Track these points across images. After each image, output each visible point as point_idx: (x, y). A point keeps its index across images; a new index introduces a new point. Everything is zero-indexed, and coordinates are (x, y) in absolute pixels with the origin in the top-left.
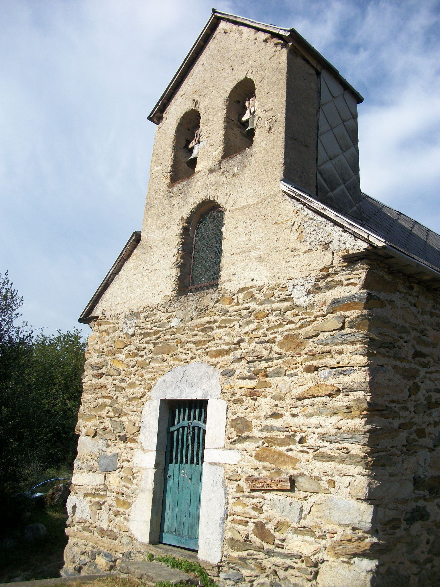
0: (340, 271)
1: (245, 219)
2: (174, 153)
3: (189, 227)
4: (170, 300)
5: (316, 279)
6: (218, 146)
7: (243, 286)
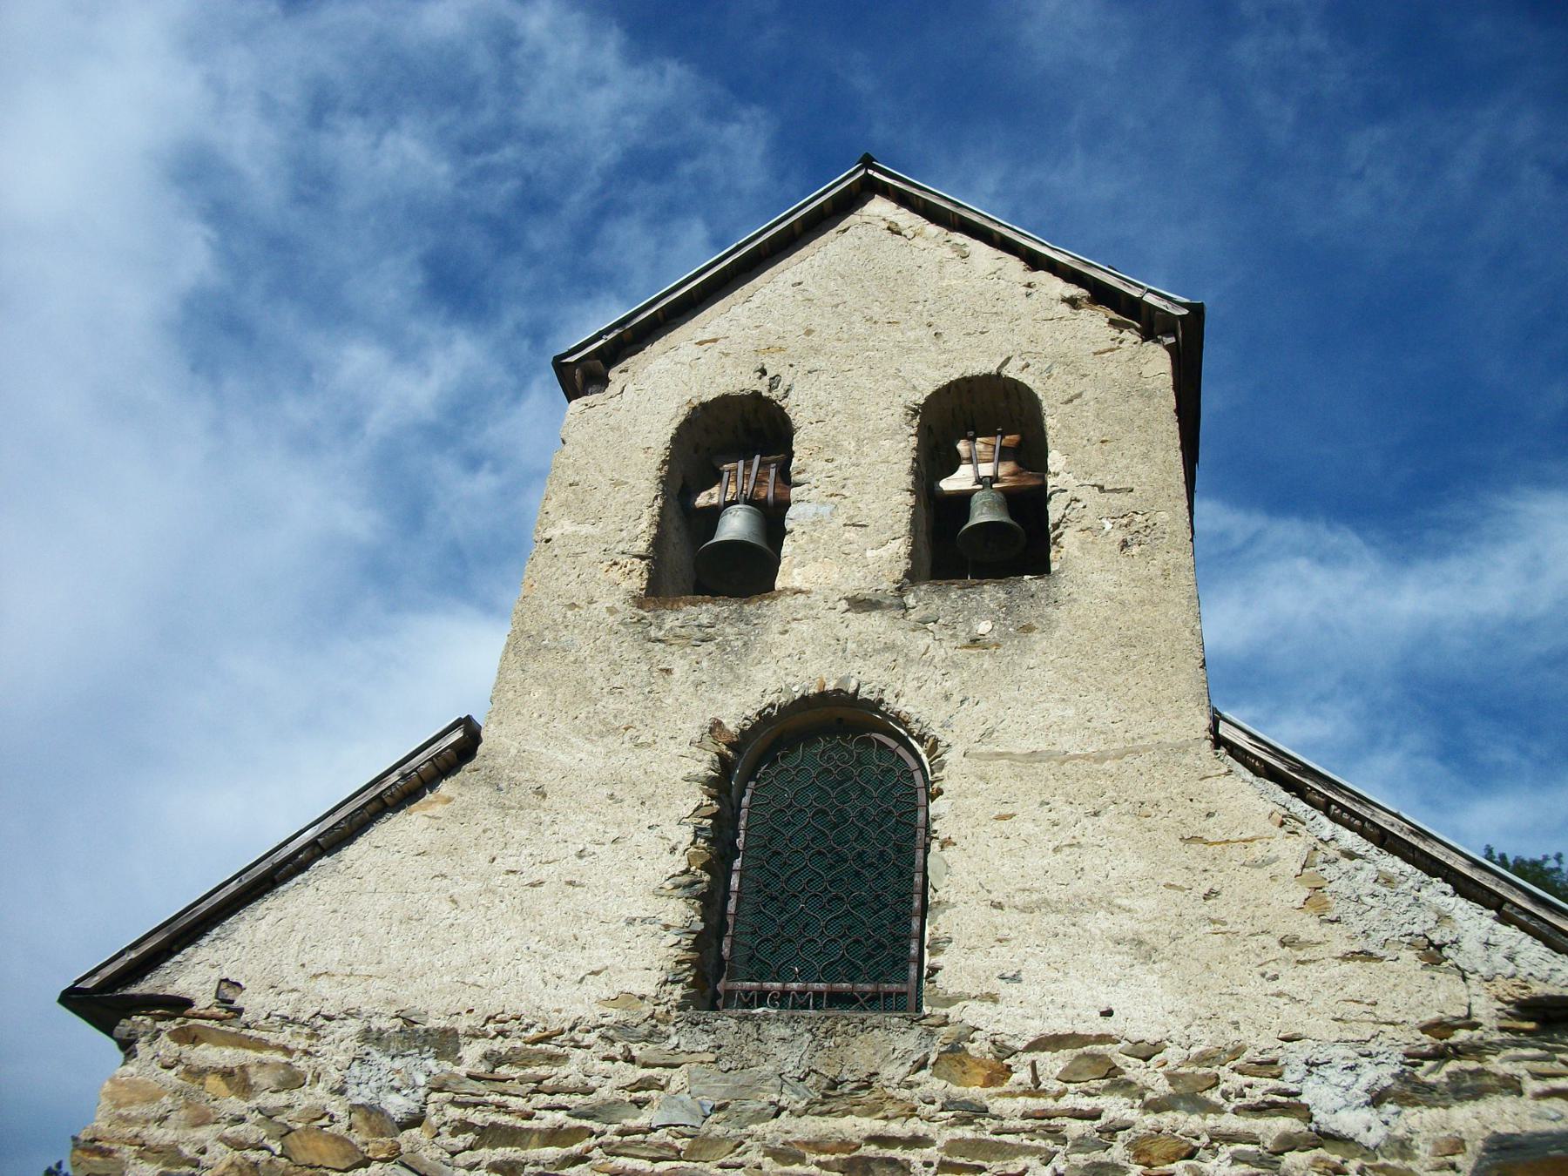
0: (1503, 1045)
1: (1046, 797)
3: (734, 764)
4: (652, 1016)
5: (1407, 1055)
6: (889, 534)
7: (1063, 1028)
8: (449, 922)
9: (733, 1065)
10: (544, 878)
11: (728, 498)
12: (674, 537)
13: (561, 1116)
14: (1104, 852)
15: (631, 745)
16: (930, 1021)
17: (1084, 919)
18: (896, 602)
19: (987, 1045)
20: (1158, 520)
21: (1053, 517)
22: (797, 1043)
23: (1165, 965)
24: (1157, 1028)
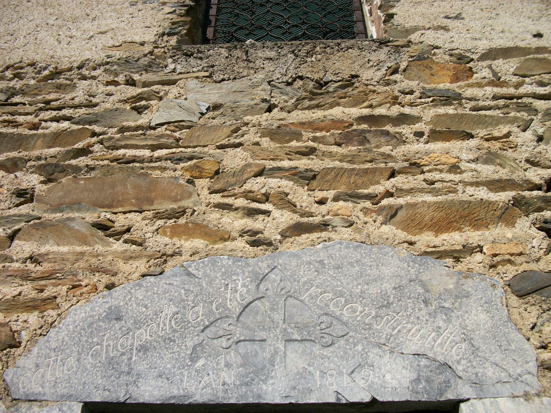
9: (226, 76)
13: (65, 125)
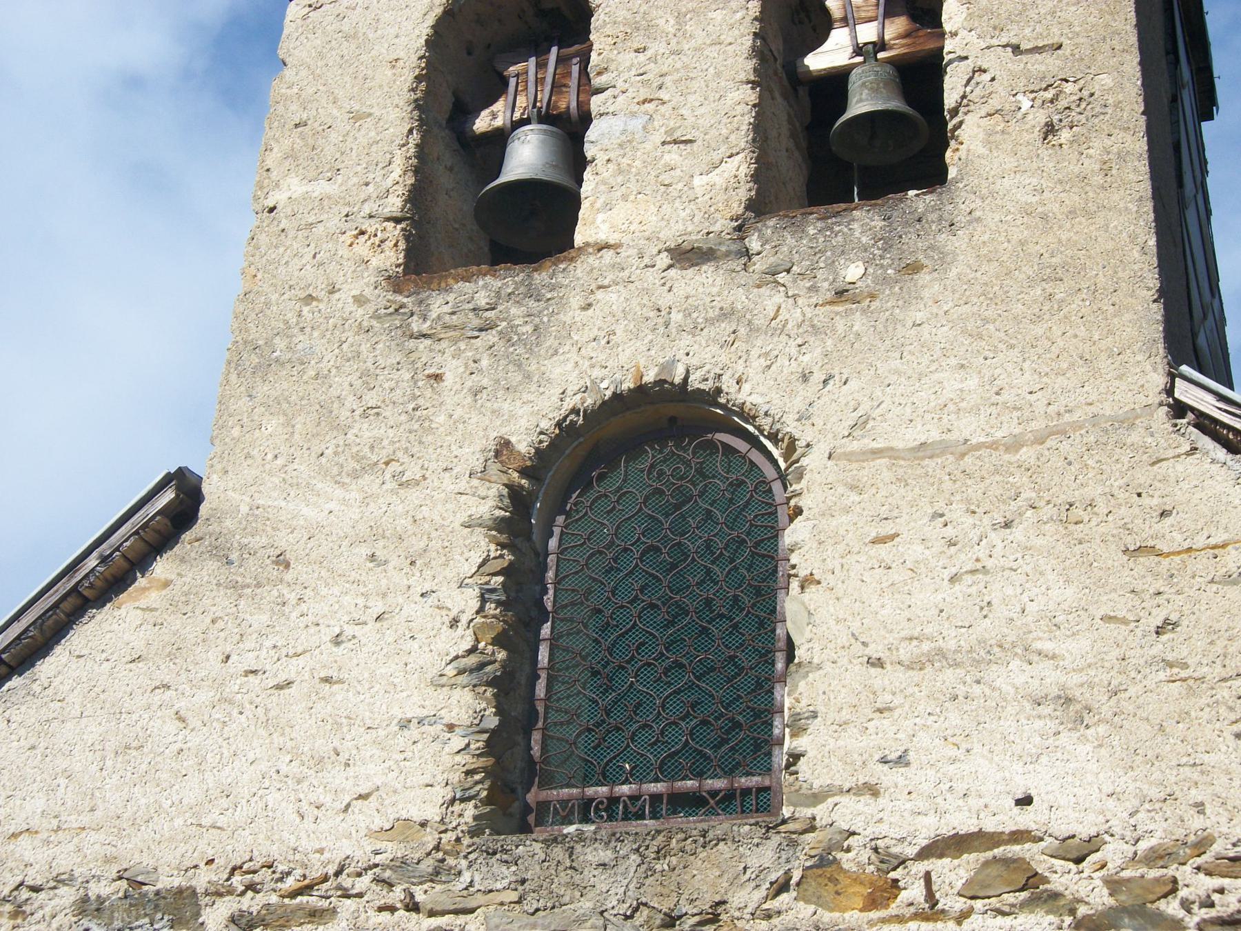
1: (940, 506)
2: (416, 137)
3: (532, 496)
4: (437, 848)
6: (724, 150)
7: (967, 825)
8: (176, 747)
9: (541, 904)
10: (293, 676)
11: (517, 115)
12: (445, 180)
14: (1018, 578)
15: (394, 485)
16: (791, 826)
17: (995, 674)
18: (734, 247)
19: (866, 854)
20: (1096, 88)
21: (950, 100)
22: (621, 869)
23: (1102, 729)
24: (1091, 817)
